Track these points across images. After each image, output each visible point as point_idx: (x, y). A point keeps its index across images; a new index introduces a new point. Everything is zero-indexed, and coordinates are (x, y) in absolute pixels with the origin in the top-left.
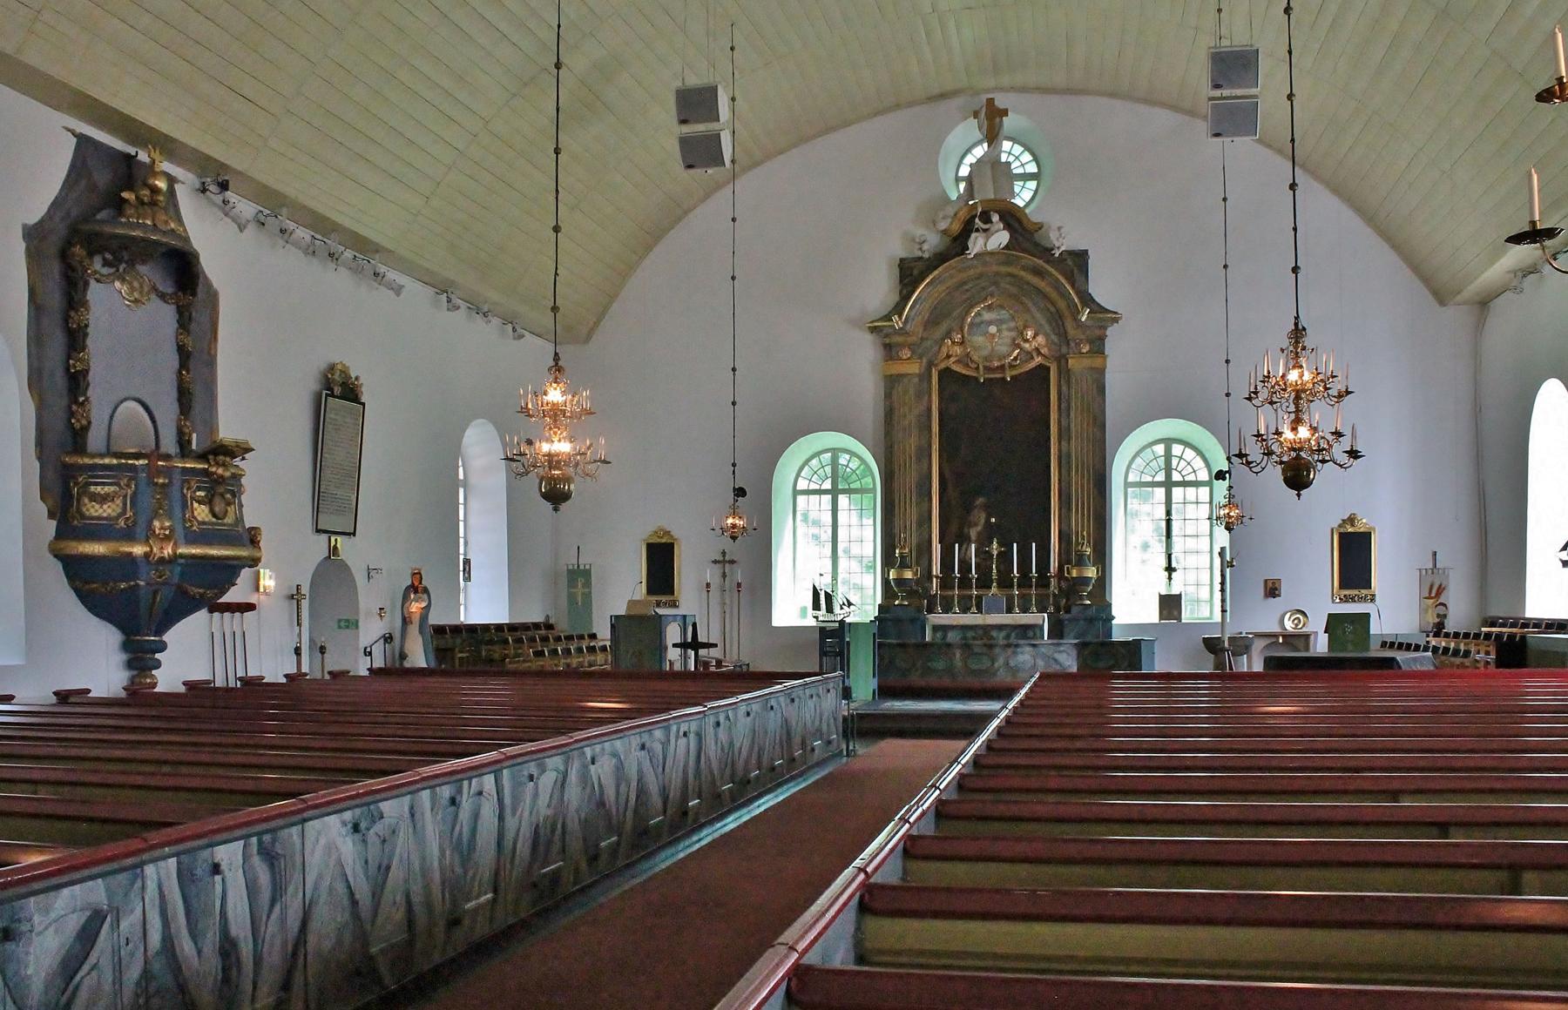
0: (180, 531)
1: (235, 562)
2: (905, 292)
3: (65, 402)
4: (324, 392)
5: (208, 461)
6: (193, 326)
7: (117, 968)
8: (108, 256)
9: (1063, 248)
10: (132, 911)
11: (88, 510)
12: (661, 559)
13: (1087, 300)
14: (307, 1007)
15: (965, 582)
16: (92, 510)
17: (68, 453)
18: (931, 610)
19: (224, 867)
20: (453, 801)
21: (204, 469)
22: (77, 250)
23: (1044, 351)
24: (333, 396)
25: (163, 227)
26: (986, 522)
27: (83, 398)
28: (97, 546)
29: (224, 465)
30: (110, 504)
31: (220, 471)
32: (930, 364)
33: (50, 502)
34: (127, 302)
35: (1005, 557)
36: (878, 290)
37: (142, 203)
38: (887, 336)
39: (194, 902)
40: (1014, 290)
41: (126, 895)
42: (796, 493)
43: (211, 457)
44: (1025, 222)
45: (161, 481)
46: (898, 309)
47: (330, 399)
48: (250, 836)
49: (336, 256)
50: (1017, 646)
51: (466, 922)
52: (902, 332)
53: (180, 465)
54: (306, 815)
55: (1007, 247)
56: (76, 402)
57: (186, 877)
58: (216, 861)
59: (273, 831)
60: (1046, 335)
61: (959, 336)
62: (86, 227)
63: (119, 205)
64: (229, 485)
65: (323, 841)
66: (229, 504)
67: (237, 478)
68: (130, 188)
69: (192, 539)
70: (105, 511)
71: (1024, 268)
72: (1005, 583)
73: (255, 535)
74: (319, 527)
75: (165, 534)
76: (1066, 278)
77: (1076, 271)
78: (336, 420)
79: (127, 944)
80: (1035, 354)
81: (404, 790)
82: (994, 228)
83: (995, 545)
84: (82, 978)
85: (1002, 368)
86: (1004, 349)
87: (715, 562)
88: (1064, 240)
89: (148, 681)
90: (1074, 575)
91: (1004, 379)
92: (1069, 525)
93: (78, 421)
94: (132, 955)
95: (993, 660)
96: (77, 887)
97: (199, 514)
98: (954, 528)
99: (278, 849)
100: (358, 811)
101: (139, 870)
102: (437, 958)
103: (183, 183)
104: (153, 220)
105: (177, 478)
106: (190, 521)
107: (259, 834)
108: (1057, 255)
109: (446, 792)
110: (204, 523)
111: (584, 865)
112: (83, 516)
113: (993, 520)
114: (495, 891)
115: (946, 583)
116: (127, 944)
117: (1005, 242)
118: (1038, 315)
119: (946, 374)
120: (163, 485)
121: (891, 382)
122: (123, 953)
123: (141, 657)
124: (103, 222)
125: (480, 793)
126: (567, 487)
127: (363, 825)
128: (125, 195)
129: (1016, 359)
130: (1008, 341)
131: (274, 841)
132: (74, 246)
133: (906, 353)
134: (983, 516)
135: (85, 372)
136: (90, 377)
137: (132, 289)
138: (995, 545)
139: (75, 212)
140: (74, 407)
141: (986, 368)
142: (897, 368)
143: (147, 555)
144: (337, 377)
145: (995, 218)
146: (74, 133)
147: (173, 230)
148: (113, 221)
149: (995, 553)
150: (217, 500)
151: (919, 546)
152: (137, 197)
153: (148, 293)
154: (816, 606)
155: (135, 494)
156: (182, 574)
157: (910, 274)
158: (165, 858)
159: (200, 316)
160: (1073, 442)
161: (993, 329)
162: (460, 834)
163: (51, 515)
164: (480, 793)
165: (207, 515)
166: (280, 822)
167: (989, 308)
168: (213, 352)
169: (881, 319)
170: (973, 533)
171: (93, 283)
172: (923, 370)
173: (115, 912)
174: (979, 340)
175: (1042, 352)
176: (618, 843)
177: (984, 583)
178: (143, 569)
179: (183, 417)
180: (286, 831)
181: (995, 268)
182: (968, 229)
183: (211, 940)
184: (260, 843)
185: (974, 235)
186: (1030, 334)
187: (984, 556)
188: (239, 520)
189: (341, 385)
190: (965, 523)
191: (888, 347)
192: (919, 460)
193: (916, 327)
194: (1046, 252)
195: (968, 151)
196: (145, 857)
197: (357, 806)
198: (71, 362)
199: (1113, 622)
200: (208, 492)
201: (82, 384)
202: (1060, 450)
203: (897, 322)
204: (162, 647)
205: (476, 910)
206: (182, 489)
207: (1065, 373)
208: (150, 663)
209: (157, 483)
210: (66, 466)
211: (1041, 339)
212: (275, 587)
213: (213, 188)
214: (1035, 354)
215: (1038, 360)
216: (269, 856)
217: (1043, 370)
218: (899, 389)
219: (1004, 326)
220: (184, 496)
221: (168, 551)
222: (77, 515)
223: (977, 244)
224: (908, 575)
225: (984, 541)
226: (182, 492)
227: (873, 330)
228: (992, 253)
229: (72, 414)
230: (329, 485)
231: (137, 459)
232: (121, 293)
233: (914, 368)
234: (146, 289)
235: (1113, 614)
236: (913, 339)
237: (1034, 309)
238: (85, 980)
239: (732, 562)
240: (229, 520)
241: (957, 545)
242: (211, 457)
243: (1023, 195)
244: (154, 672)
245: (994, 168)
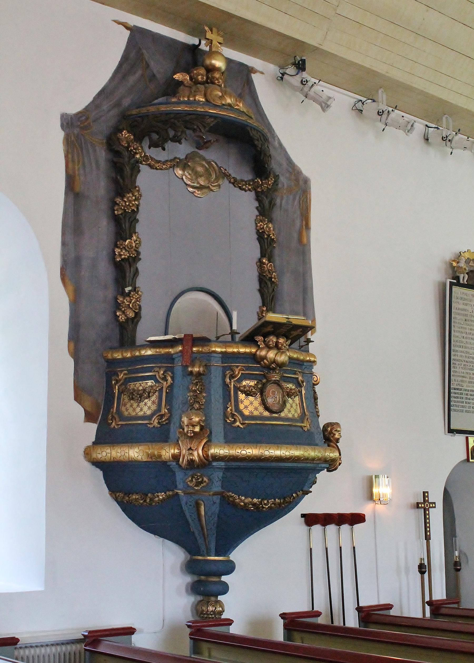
3: (110, 293)
4: (448, 281)
5: (256, 343)
8: (155, 136)
11: (127, 410)
16: (131, 410)
17: (113, 349)
21: (250, 353)
24: (458, 284)
27: (130, 288)
28: (109, 451)
30: (146, 400)
31: (271, 355)
33: (88, 404)
34: (191, 189)
37: (197, 82)
43: (259, 339)
45: (196, 369)
47: (455, 289)
49: (450, 138)
53: (219, 350)
56: (124, 294)
64: (286, 371)
73: (331, 432)
74: (452, 427)
75: (194, 432)
78: (465, 310)
89: (211, 608)
93: (123, 312)
97: (246, 407)
103: (262, 73)
104: (205, 96)
105: (216, 363)
106: (233, 415)
112: (122, 417)
120: (199, 374)
132: (121, 131)
136: (140, 265)
139: (126, 102)
140: (120, 299)
143: (176, 458)
144: (462, 264)
146: (127, 28)
147: (229, 105)
150: (271, 389)
152: (191, 79)
153: (217, 179)
155: (171, 387)
156: (224, 481)
163: (89, 417)
165: (256, 409)
168: (305, 240)
171: (143, 168)
178: (179, 475)
179: (265, 309)
189: (467, 273)
198: (117, 251)
200: (259, 381)
201: (128, 274)
206: (224, 376)
208: (214, 588)
209: (191, 373)
210: (111, 363)
212: (392, 494)
213: (291, 70)
220: (226, 386)
221: (198, 454)
222: (116, 416)
226: (224, 382)
229: (118, 306)
230: (462, 381)
231: (172, 347)
232: (182, 179)
242: (259, 339)
244: (220, 598)
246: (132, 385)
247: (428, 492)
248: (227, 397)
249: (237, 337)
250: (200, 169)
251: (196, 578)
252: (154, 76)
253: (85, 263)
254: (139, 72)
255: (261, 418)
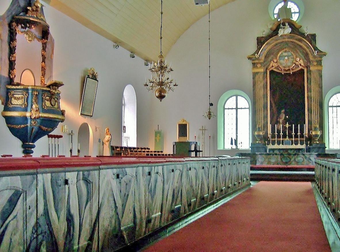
0: (41, 109)
1: (58, 120)
2: (259, 47)
6: (46, 49)
7: (25, 219)
8: (23, 25)
9: (308, 33)
10: (32, 194)
12: (183, 129)
13: (316, 49)
14: (98, 250)
15: (279, 136)
18: (268, 144)
19: (69, 182)
20: (149, 174)
22: (14, 24)
23: (302, 64)
24: (89, 78)
25: (40, 18)
26: (285, 118)
29: (55, 89)
31: (54, 91)
32: (267, 69)
35: (290, 129)
36: (252, 47)
37: (33, 11)
38: (253, 60)
39: (57, 195)
40: (292, 46)
41: (29, 187)
42: (237, 96)
44: (296, 25)
46: (257, 52)
48: (80, 171)
50: (298, 155)
51: (153, 221)
52: (258, 59)
54: (101, 167)
55: (290, 33)
57: (54, 183)
58: (66, 178)
59: (88, 171)
60: (303, 60)
61: (276, 60)
62: (17, 17)
63: (26, 11)
65: (106, 179)
66: (56, 101)
67: (58, 94)
68: (30, 6)
69: (45, 111)
70: (18, 103)
71: (296, 40)
72: (290, 136)
76: (309, 42)
77: (312, 40)
79: (30, 209)
80: (300, 66)
81: (134, 165)
82: (286, 27)
83: (287, 124)
84: (9, 222)
85: (289, 70)
86: (289, 64)
87: (200, 130)
88: (308, 30)
90: (313, 134)
91: (290, 73)
92: (311, 118)
94: (31, 214)
95: (290, 159)
96: (9, 178)
98: (275, 121)
99: (90, 178)
100: (118, 170)
101: (35, 176)
102: (143, 236)
104: (36, 15)
107: (83, 171)
108: (306, 35)
109: (147, 169)
110: (49, 107)
111: (187, 207)
113: (287, 117)
114: (161, 212)
115: (273, 136)
116: (30, 209)
117: (290, 31)
118: (300, 54)
119: (272, 72)
121: (255, 74)
122: (27, 212)
123: (27, 150)
124: (21, 15)
125: (157, 173)
126: (164, 94)
127: (120, 176)
128: (29, 8)
129: (294, 67)
130: (291, 62)
131: (89, 175)
133: (259, 66)
134: (284, 115)
135: (15, 61)
137: (29, 37)
138: (287, 124)
139: (13, 13)
141: (284, 70)
142: (256, 70)
145: (287, 24)
148: (25, 15)
149: (287, 127)
150: (53, 99)
151: (264, 125)
154: (232, 144)
157: (260, 42)
158: (46, 173)
159: (48, 46)
160: (312, 92)
161: (286, 58)
162: (151, 188)
163: (3, 104)
164: (157, 173)
166: (92, 168)
167: (286, 52)
169: (252, 55)
170: (281, 121)
172: (264, 71)
173: (25, 193)
174: (282, 61)
175: (302, 65)
176: (208, 196)
177: (284, 136)
178: (29, 121)
180: (94, 172)
181: (287, 40)
182: (278, 28)
183: (63, 214)
184: (83, 175)
185: (280, 29)
186: (298, 59)
187: (284, 128)
188: (59, 107)
190: (278, 117)
191: (254, 64)
192: (264, 98)
193: (263, 58)
194: (303, 35)
195: (277, 5)
196: (39, 170)
197: (119, 168)
199: (326, 149)
202: (308, 95)
203: (257, 56)
204: (33, 147)
205: (156, 217)
206: (42, 96)
207: (309, 72)
210: (8, 89)
211: (301, 61)
214: (300, 66)
215: (300, 67)
216: (87, 181)
217: (302, 71)
218: (257, 77)
219: (290, 57)
223: (281, 32)
224: (261, 133)
225: (284, 123)
227: (249, 58)
228: (285, 35)
233: (262, 70)
234: (33, 37)
235: (326, 146)
236: (262, 61)
237: (299, 52)
238: (11, 223)
239: (205, 130)
240: (56, 106)
241: (276, 125)
243: (295, 18)
245: (286, 11)
246: (15, 96)
247: (258, 39)
248: (43, 101)
249: (45, 86)
250: (30, 35)
251: (25, 149)
252: (20, 6)
253: (3, 60)
254: (16, 5)
255: (50, 107)
